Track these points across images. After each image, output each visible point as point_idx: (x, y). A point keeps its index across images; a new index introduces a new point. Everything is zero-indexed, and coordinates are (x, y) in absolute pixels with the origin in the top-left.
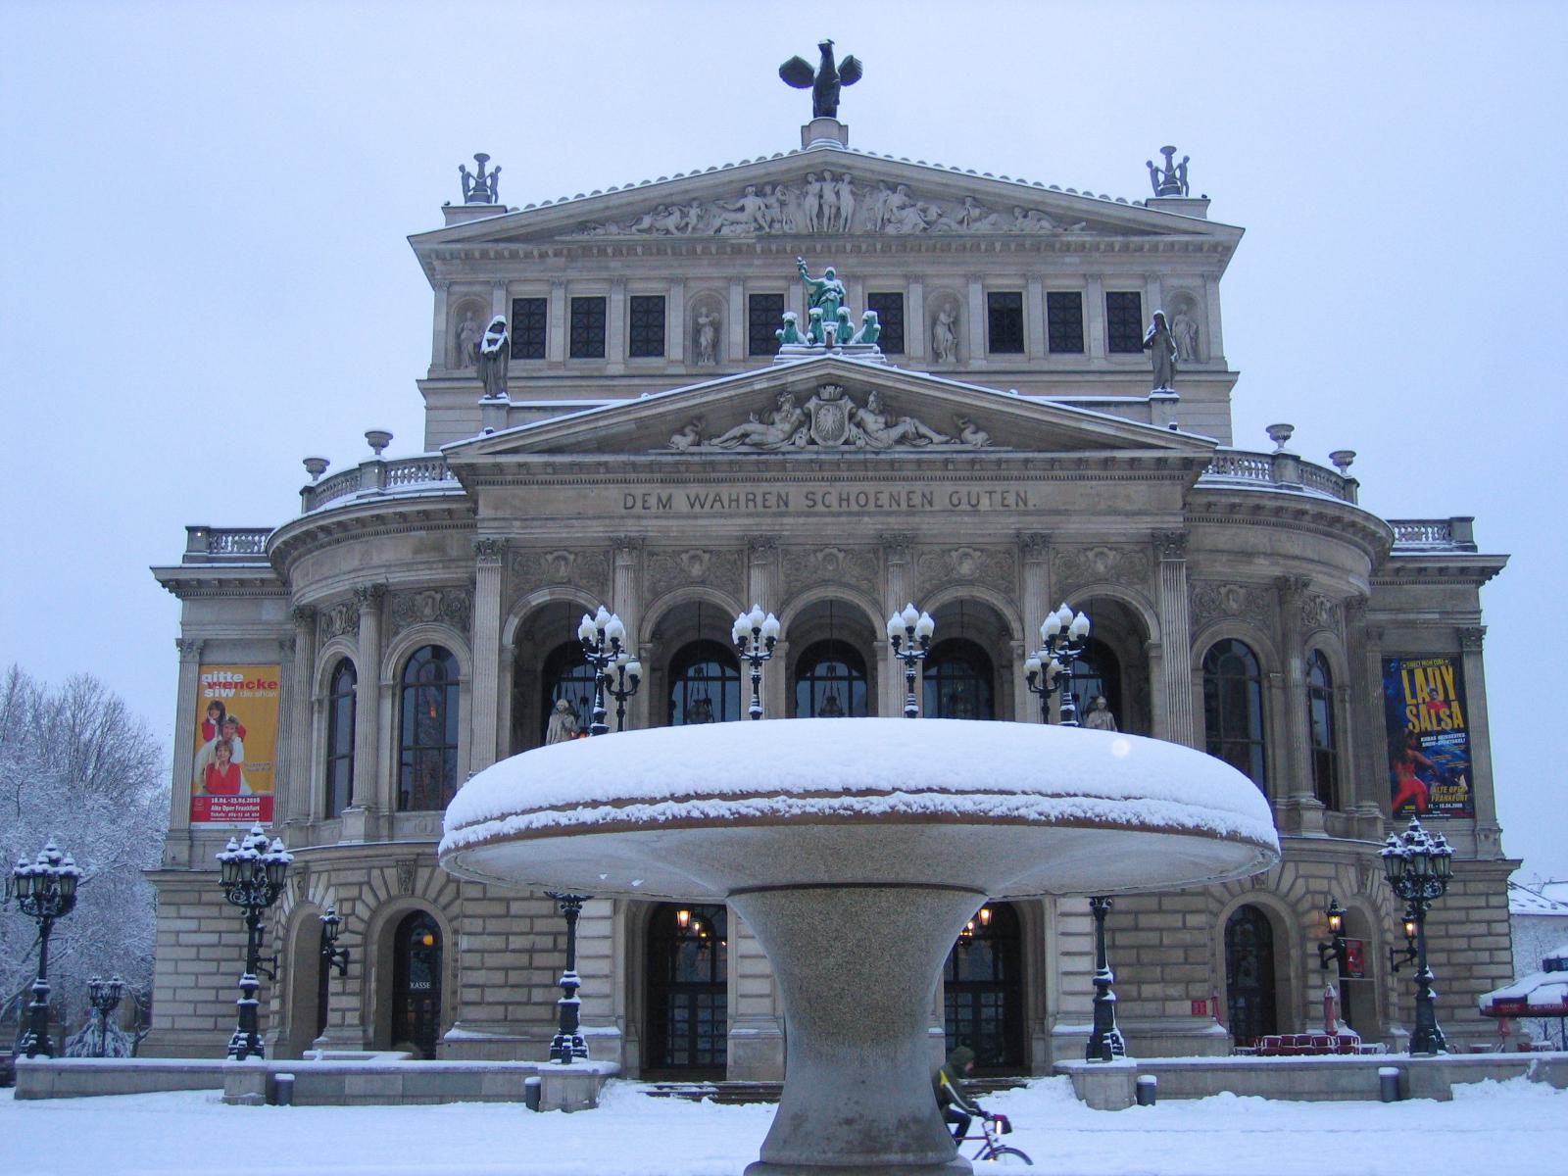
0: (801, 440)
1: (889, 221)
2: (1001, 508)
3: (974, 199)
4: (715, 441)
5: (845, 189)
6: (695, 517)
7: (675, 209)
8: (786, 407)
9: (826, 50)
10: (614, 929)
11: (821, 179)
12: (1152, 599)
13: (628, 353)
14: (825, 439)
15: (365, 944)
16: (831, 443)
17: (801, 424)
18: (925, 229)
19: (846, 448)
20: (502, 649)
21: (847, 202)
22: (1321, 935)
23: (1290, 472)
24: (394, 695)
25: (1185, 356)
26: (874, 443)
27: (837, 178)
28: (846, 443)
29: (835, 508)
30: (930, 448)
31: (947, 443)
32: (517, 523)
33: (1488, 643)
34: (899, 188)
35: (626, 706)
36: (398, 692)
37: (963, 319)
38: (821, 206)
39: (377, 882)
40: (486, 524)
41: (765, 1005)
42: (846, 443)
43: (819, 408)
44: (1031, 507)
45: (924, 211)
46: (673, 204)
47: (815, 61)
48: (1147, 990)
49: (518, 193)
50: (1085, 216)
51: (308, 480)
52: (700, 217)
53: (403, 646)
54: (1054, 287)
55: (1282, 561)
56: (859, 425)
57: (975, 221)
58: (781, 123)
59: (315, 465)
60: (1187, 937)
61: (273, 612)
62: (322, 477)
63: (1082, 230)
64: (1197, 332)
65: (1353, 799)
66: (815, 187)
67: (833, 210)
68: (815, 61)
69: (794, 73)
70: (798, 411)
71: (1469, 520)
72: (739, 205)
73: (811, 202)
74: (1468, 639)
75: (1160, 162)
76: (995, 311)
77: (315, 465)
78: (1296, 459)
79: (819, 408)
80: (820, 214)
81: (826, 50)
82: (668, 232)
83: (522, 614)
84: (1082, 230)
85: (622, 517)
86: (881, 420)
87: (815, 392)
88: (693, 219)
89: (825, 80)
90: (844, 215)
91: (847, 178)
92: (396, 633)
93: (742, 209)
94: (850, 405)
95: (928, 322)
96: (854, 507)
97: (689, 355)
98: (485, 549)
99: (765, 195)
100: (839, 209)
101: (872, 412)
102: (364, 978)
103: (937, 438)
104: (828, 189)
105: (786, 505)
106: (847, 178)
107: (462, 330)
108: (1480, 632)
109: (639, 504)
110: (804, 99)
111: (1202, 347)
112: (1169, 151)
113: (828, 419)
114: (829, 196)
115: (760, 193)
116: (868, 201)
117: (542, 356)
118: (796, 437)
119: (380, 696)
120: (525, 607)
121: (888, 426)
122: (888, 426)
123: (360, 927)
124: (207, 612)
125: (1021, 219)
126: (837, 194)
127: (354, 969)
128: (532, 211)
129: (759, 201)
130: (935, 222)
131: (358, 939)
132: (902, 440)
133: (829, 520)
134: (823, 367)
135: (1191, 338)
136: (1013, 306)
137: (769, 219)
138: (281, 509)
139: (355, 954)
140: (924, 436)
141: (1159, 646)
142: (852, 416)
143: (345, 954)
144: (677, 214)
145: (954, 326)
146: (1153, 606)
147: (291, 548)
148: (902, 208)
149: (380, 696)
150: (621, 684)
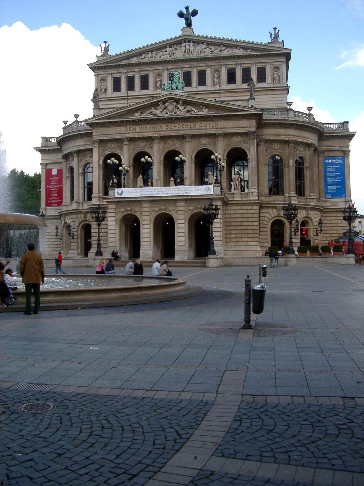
0: (164, 113)
1: (202, 52)
2: (212, 127)
3: (223, 45)
4: (145, 114)
5: (191, 44)
6: (141, 132)
7: (150, 52)
8: (161, 105)
9: (187, 8)
10: (150, 226)
11: (185, 42)
12: (249, 147)
13: (140, 89)
14: (170, 112)
15: (77, 231)
16: (171, 113)
17: (165, 109)
18: (211, 54)
19: (175, 114)
20: (99, 165)
21: (192, 48)
22: (295, 227)
23: (291, 113)
24: (82, 175)
25: (276, 82)
26: (181, 113)
27: (189, 42)
28: (175, 113)
29: (173, 129)
30: (194, 113)
31: (198, 112)
32: (101, 136)
33: (351, 154)
34: (205, 43)
35: (125, 177)
36: (83, 174)
37: (221, 76)
38: (185, 49)
39: (79, 218)
40: (94, 136)
41: (183, 243)
42: (175, 113)
43: (168, 105)
44: (219, 127)
45: (211, 49)
46: (149, 51)
47: (185, 11)
48: (244, 240)
49: (113, 52)
50: (251, 48)
51: (64, 125)
52: (156, 54)
53: (84, 164)
54: (244, 66)
55: (288, 136)
56: (178, 109)
57: (223, 51)
58: (175, 29)
59: (65, 122)
60: (253, 227)
61: (60, 156)
62: (67, 125)
63: (250, 51)
64: (280, 76)
65: (308, 194)
66: (184, 45)
67: (188, 50)
68: (185, 11)
69: (181, 15)
70: (164, 106)
71: (348, 122)
72: (165, 50)
73: (183, 49)
74: (346, 153)
75: (273, 32)
76: (229, 73)
77: (65, 122)
78: (293, 110)
79: (168, 105)
80: (185, 52)
81: (187, 8)
82: (149, 58)
83: (104, 156)
84: (250, 51)
85: (125, 133)
86: (183, 107)
87: (167, 101)
88: (154, 55)
89: (187, 16)
90: (191, 51)
91: (192, 41)
92: (82, 161)
93: (166, 51)
94: (176, 104)
95: (212, 77)
96: (177, 129)
97: (155, 88)
98: (95, 142)
99: (172, 47)
100: (190, 50)
101: (181, 105)
102: (77, 239)
103: (196, 111)
104: (187, 44)
105: (162, 128)
106: (192, 41)
107: (101, 86)
108: (349, 151)
109: (128, 130)
110: (183, 20)
111: (281, 80)
112: (275, 29)
113: (170, 107)
114: (187, 47)
115: (170, 47)
116: (197, 47)
117: (120, 91)
118: (163, 113)
119: (79, 176)
120: (104, 155)
121: (185, 108)
122: (185, 108)
123: (76, 228)
124: (47, 156)
125: (235, 49)
126: (189, 46)
127: (75, 237)
128: (117, 55)
129: (170, 49)
130: (213, 52)
131: (76, 230)
132: (188, 111)
133: (171, 132)
134: (169, 95)
135: (278, 78)
136: (233, 72)
137: (172, 53)
138: (59, 133)
139: (75, 233)
140: (193, 111)
141: (250, 159)
142: (176, 107)
143: (73, 234)
144: (151, 53)
145: (219, 77)
146: (248, 149)
147: (61, 141)
148: (205, 48)
149: (79, 176)
150: (124, 172)
